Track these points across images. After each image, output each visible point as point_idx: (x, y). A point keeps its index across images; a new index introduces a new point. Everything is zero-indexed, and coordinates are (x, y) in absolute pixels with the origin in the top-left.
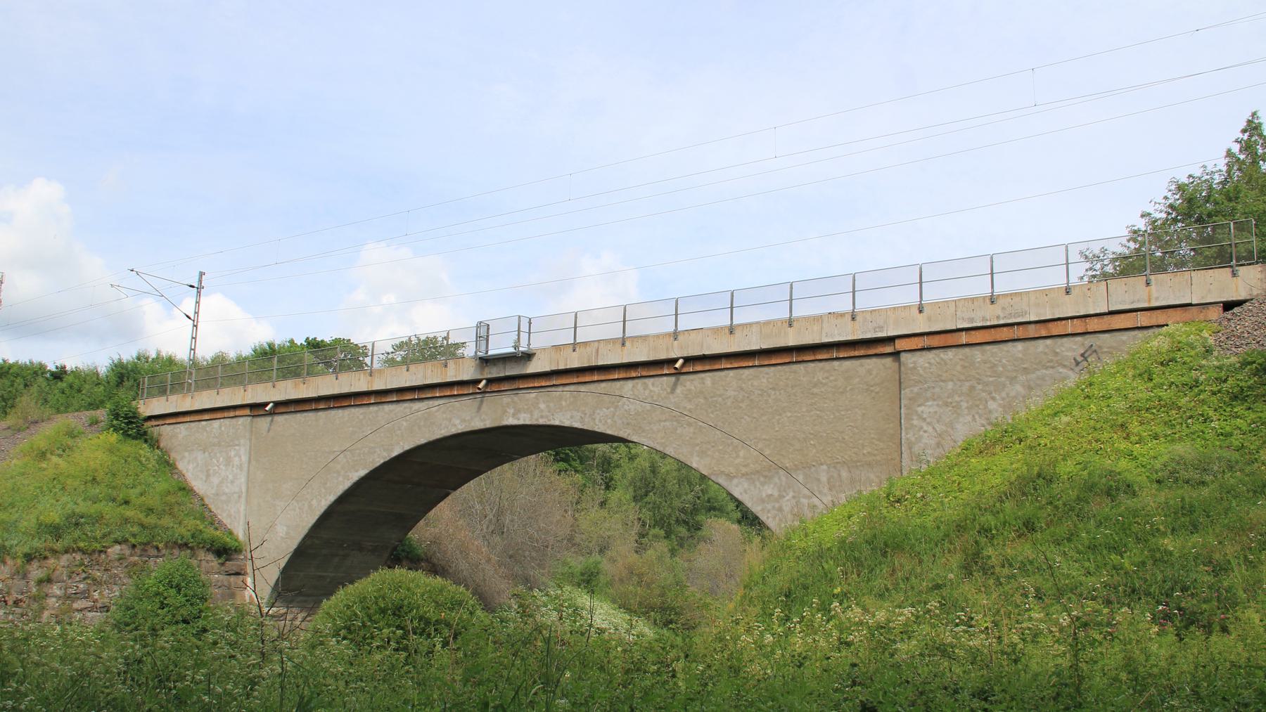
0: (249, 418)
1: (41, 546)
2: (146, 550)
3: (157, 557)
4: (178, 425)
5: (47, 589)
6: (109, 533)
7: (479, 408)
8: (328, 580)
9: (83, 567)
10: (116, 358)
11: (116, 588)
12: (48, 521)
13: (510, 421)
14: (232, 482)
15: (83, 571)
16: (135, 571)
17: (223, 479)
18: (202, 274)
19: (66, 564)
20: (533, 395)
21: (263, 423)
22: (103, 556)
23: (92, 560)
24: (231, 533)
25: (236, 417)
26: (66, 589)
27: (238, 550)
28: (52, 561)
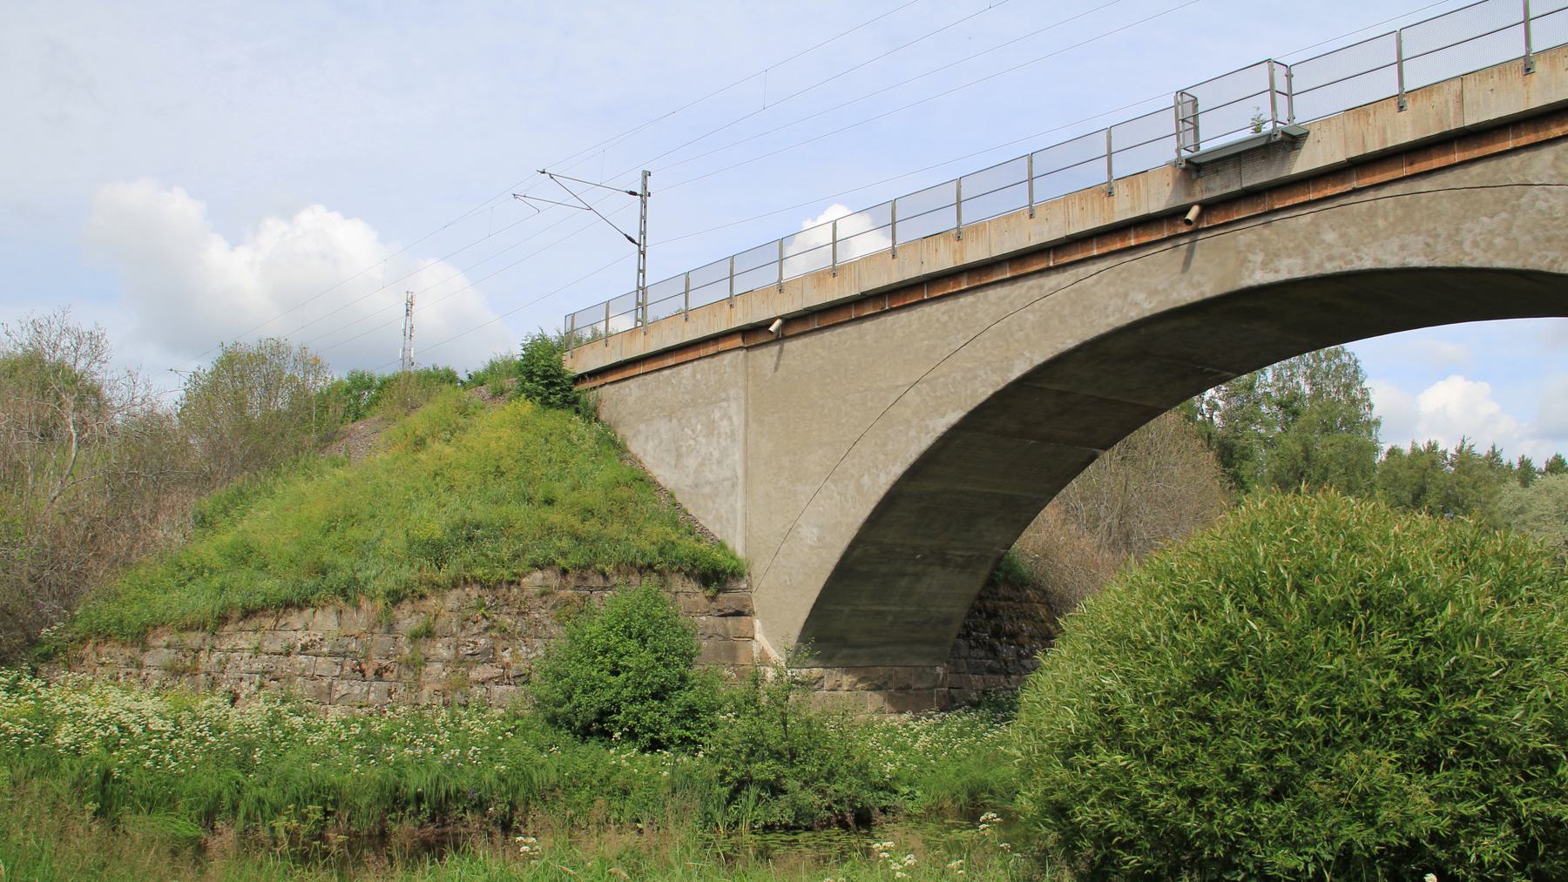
0: (742, 353)
1: (413, 577)
2: (585, 579)
3: (604, 589)
4: (626, 383)
5: (426, 648)
6: (524, 552)
7: (1187, 263)
8: (890, 618)
9: (482, 610)
10: (536, 333)
11: (538, 643)
12: (422, 535)
13: (1259, 277)
14: (719, 462)
15: (484, 616)
16: (569, 613)
17: (703, 459)
18: (646, 175)
19: (455, 607)
20: (1305, 218)
21: (766, 356)
22: (515, 590)
23: (497, 598)
24: (723, 546)
25: (719, 353)
26: (457, 647)
27: (736, 574)
28: (432, 602)
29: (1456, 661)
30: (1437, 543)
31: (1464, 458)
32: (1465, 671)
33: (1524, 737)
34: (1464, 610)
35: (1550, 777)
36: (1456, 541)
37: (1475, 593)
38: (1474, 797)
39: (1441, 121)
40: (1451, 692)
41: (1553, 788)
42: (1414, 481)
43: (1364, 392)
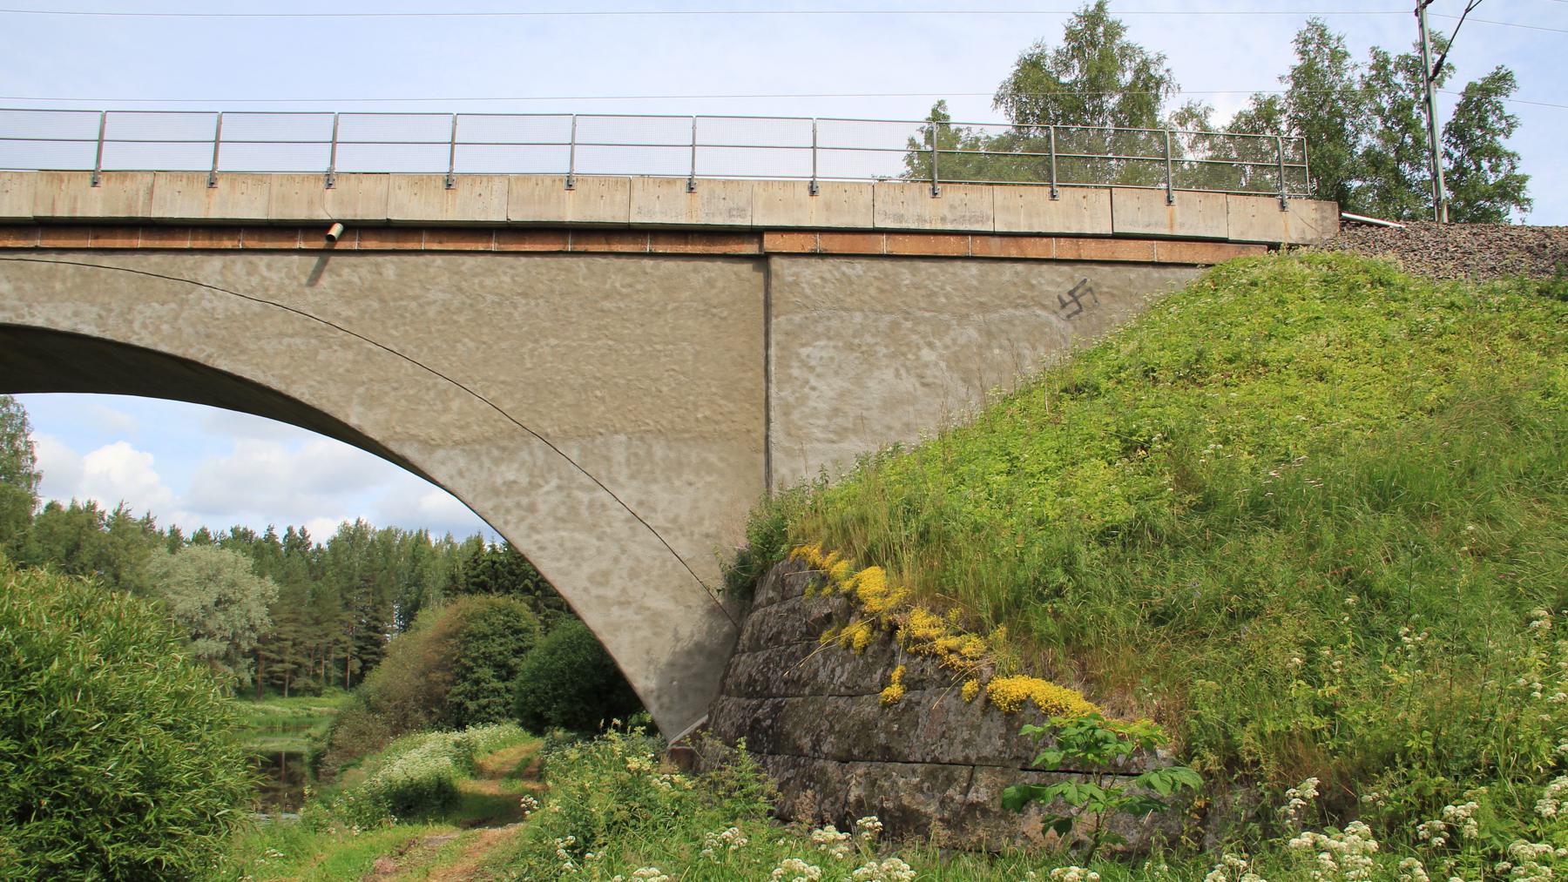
29: (58, 715)
30: (53, 600)
31: (121, 521)
32: (65, 724)
33: (117, 786)
34: (71, 665)
35: (138, 822)
36: (74, 599)
37: (85, 650)
38: (63, 845)
39: (130, 206)
40: (50, 743)
41: (141, 834)
42: (70, 536)
43: (29, 444)
